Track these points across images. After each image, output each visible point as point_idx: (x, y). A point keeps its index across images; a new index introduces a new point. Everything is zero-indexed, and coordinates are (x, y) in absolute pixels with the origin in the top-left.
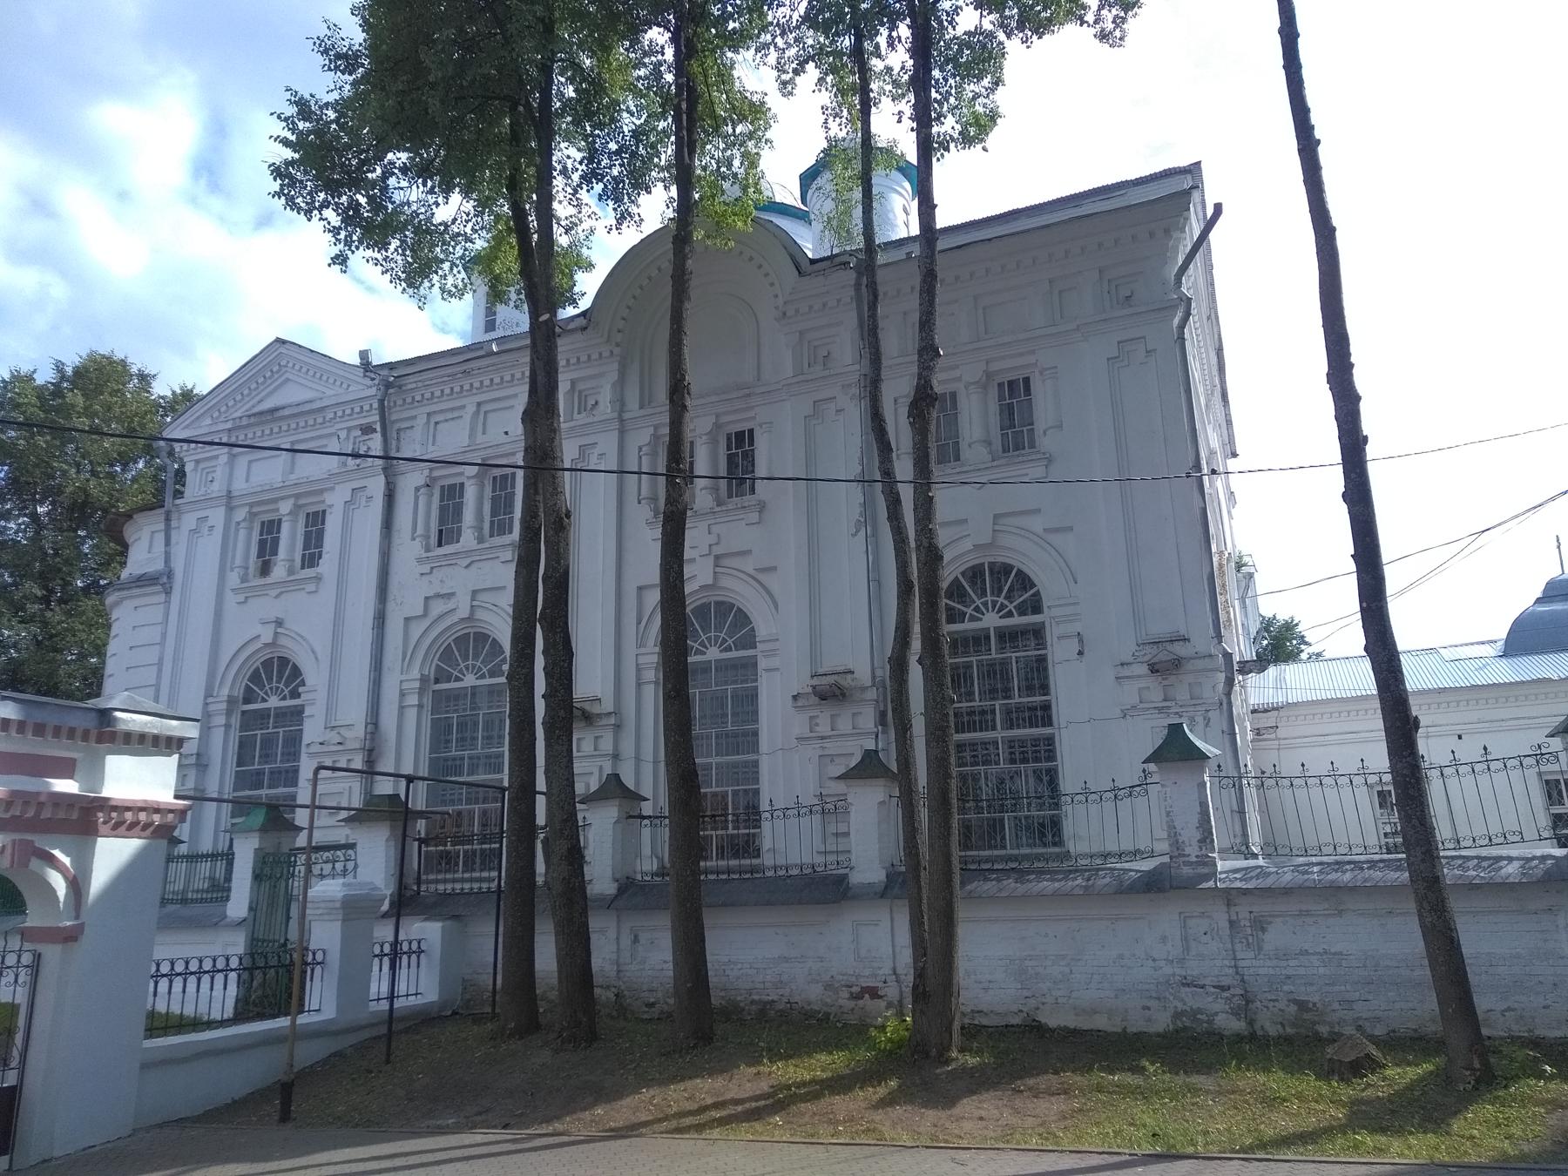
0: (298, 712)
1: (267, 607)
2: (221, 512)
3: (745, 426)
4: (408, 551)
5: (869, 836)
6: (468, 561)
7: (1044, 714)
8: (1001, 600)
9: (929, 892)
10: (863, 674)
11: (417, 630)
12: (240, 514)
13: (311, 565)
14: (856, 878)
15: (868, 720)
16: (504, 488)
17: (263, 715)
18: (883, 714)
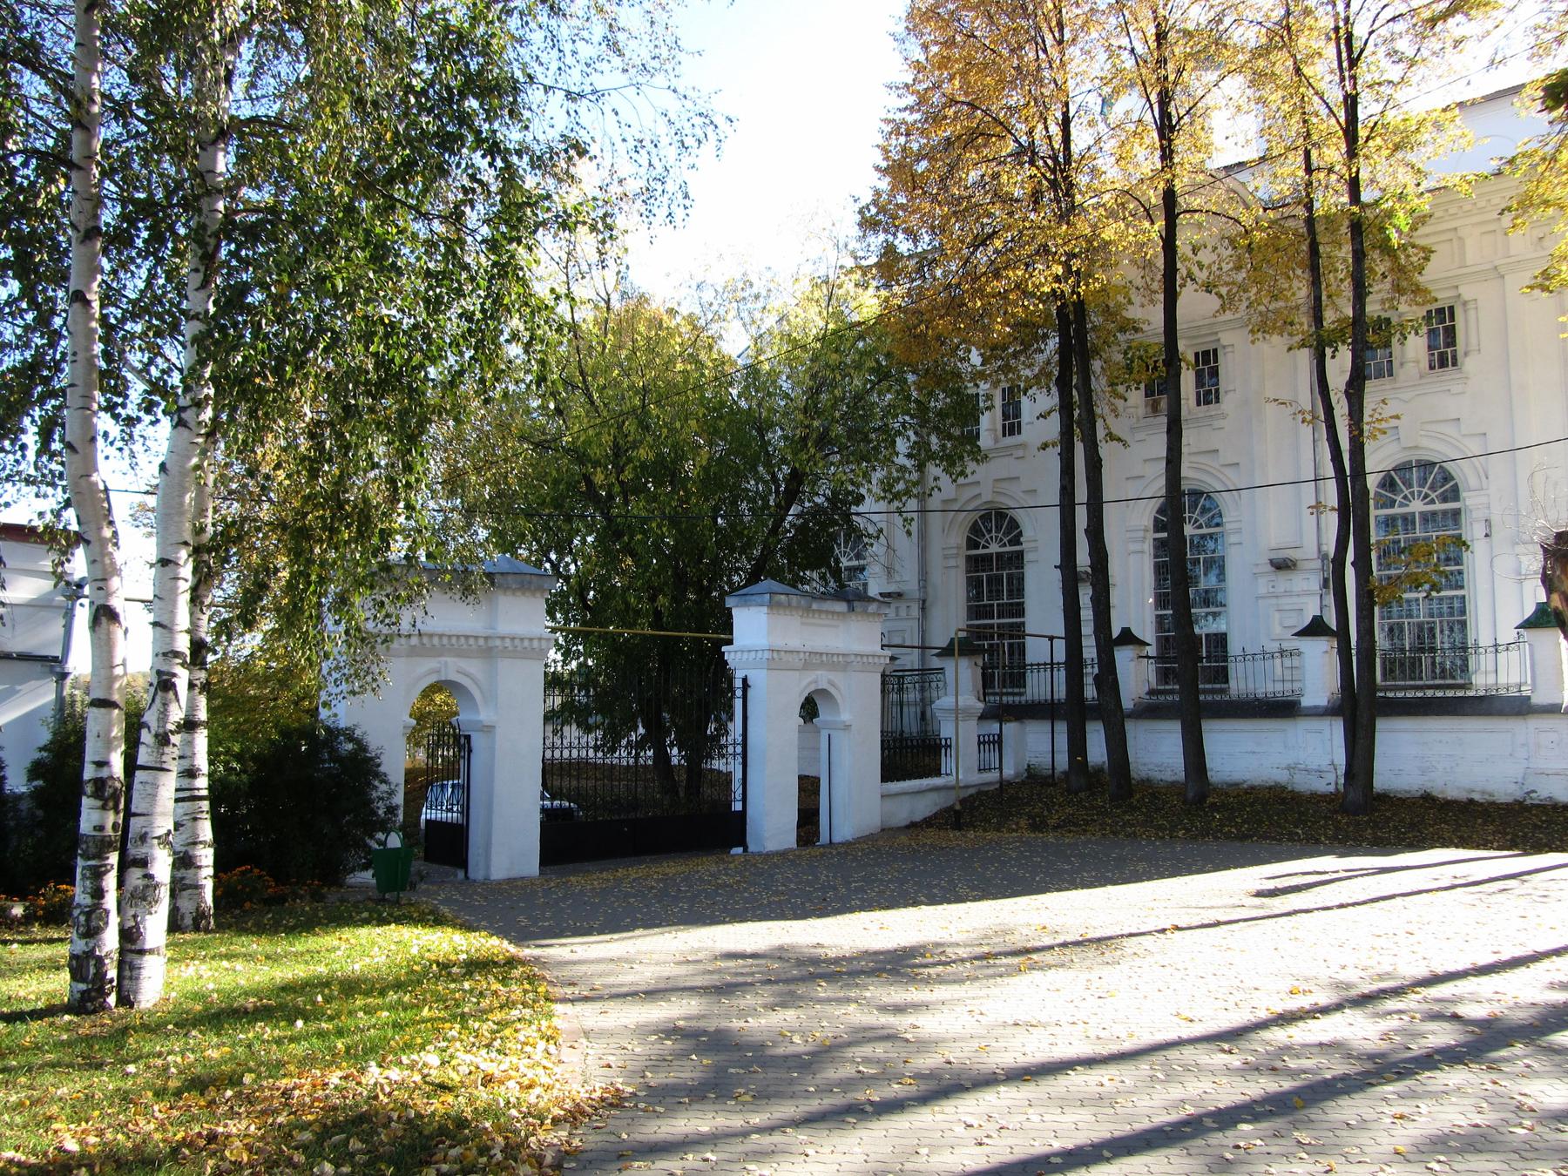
0: (1017, 559)
3: (1210, 347)
5: (1318, 674)
7: (1019, 610)
8: (1425, 490)
9: (1359, 710)
10: (1310, 550)
13: (1012, 433)
14: (1306, 702)
15: (1314, 583)
16: (1206, 362)
17: (987, 558)
18: (1326, 581)
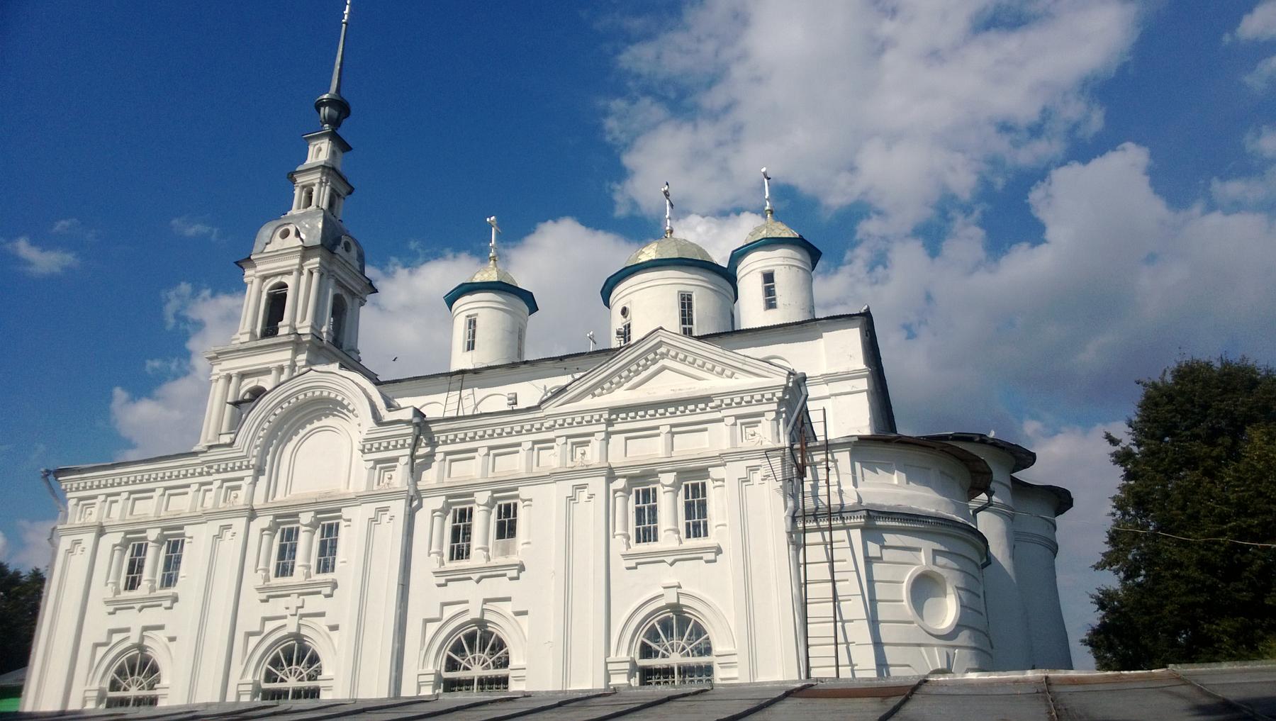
1: (134, 620)
2: (602, 481)
4: (425, 564)
6: (672, 559)
11: (432, 628)
12: (620, 483)
17: (124, 702)
